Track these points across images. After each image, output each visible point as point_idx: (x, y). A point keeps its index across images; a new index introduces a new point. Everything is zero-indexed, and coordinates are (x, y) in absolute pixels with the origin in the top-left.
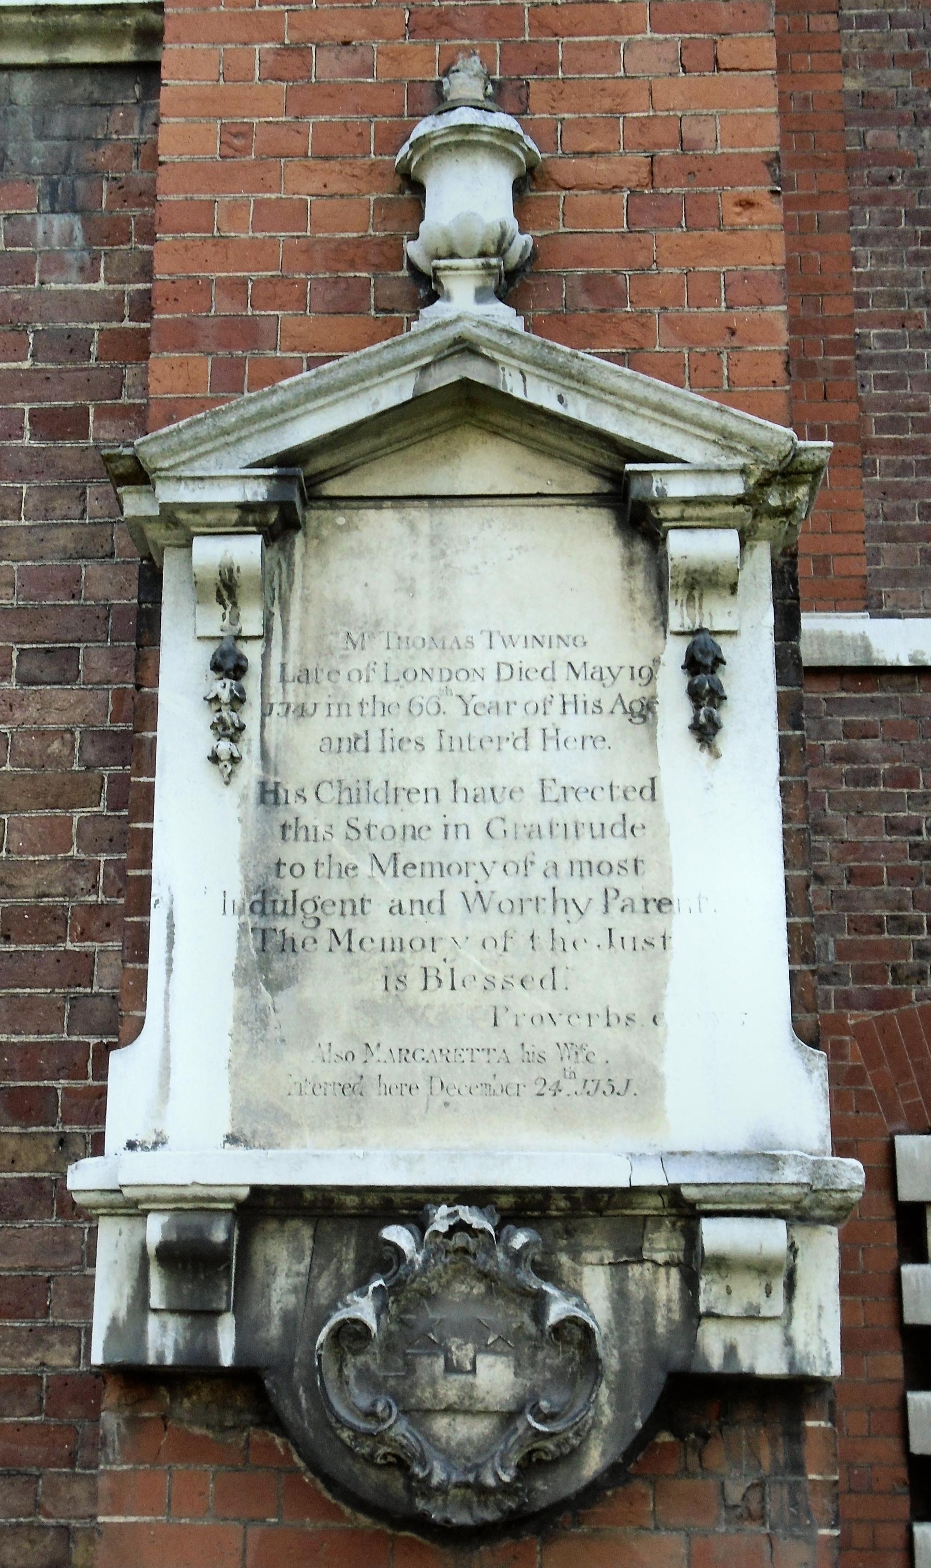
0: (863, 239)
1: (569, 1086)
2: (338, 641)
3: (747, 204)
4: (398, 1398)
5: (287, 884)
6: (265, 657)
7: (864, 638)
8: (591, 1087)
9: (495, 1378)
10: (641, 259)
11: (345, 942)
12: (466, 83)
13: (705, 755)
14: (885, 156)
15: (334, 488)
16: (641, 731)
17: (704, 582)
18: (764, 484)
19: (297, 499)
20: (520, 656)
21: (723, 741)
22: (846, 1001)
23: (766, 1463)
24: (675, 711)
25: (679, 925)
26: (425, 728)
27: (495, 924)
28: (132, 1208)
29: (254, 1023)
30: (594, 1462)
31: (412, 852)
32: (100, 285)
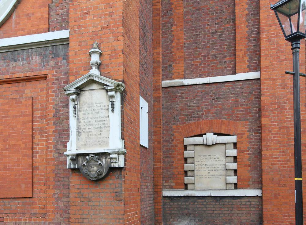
0: (186, 31)
1: (102, 144)
2: (83, 104)
3: (120, 55)
4: (88, 170)
5: (80, 127)
6: (78, 106)
7: (183, 82)
8: (104, 144)
9: (95, 168)
10: (111, 62)
11: (85, 132)
12: (95, 46)
13: (113, 113)
14: (188, 19)
15: (83, 90)
16: (107, 111)
17: (112, 97)
18: (116, 87)
19: (79, 91)
20: (98, 105)
21: (114, 112)
22: (180, 124)
23: (119, 174)
24: (110, 109)
25: (111, 129)
26: (90, 112)
27: (96, 130)
28: (68, 156)
29: (78, 139)
30: (104, 174)
31: (90, 124)
32: (68, 68)
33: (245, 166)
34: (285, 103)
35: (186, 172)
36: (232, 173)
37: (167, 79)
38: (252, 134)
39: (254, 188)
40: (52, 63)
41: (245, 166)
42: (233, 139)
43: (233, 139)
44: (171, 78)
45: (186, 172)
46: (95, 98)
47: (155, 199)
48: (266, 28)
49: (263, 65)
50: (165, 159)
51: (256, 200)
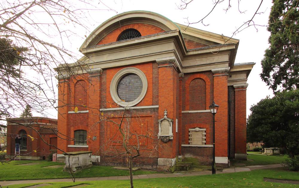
17: (170, 123)
19: (162, 121)
33: (209, 138)
34: (221, 120)
35: (189, 139)
37: (183, 110)
38: (211, 128)
39: (211, 144)
40: (153, 113)
41: (209, 138)
42: (205, 129)
43: (205, 129)
44: (185, 110)
45: (189, 139)
46: (166, 123)
47: (179, 147)
48: (216, 97)
50: (182, 135)
51: (211, 148)
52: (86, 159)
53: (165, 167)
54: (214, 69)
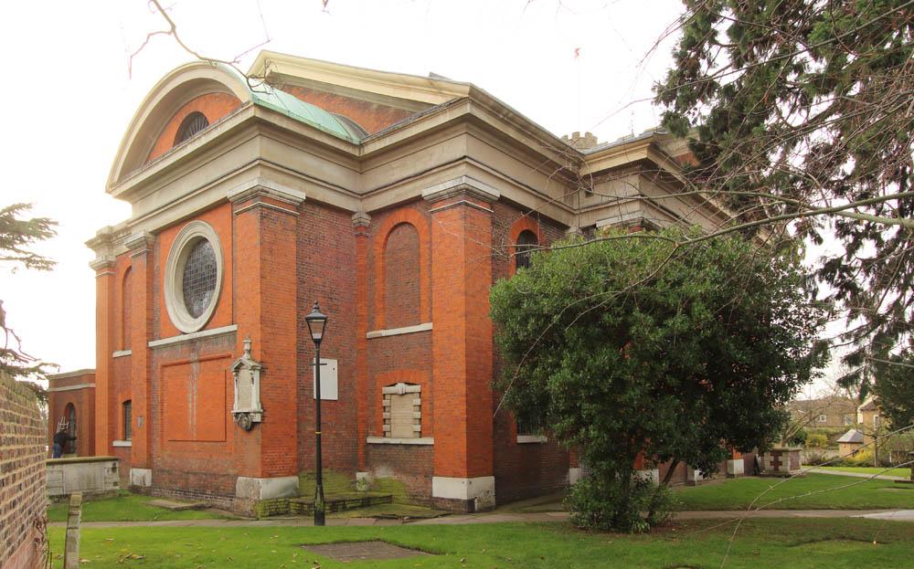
36: (418, 422)
37: (372, 330)
42: (417, 388)
49: (434, 318)
52: (94, 478)
53: (247, 501)
54: (428, 189)
